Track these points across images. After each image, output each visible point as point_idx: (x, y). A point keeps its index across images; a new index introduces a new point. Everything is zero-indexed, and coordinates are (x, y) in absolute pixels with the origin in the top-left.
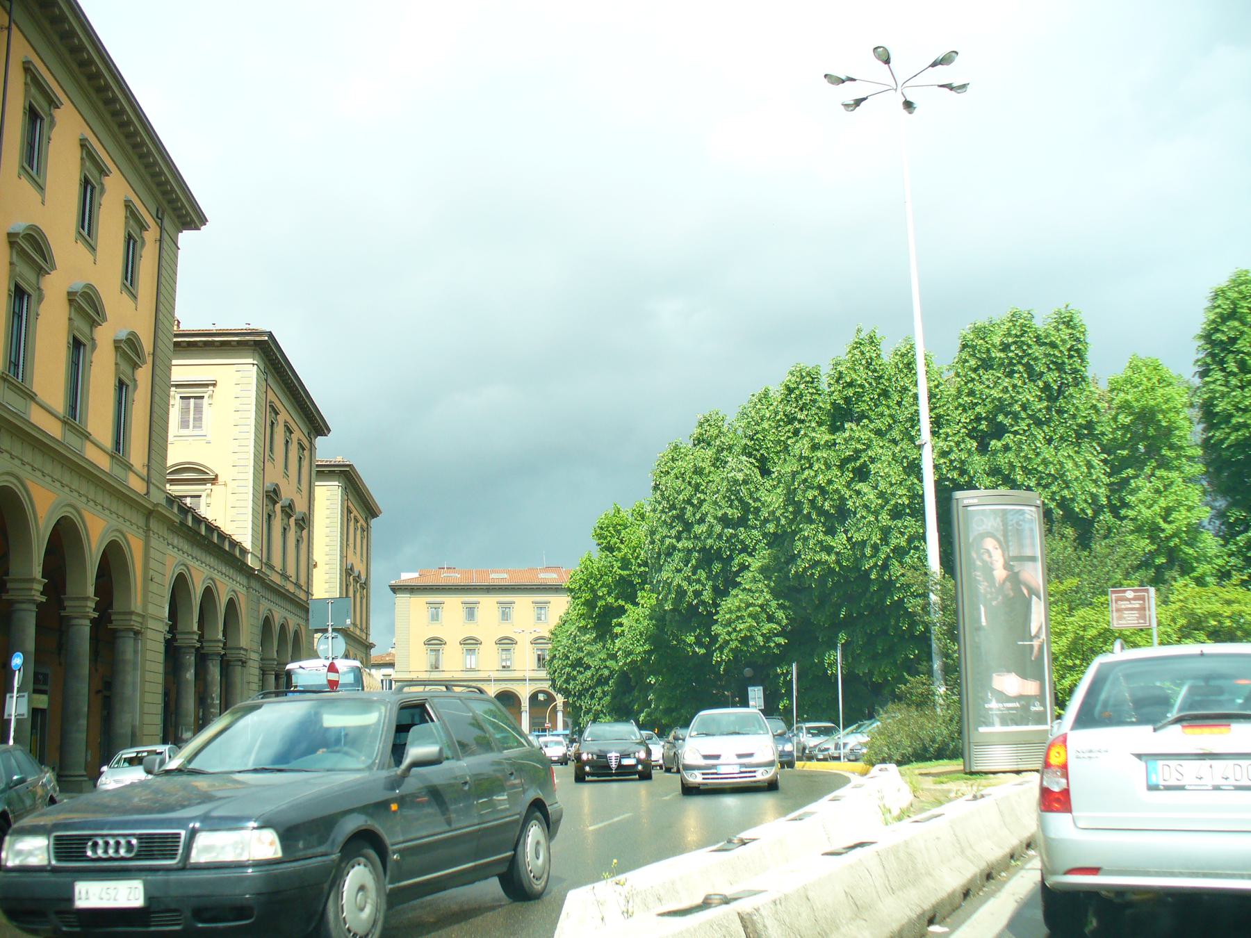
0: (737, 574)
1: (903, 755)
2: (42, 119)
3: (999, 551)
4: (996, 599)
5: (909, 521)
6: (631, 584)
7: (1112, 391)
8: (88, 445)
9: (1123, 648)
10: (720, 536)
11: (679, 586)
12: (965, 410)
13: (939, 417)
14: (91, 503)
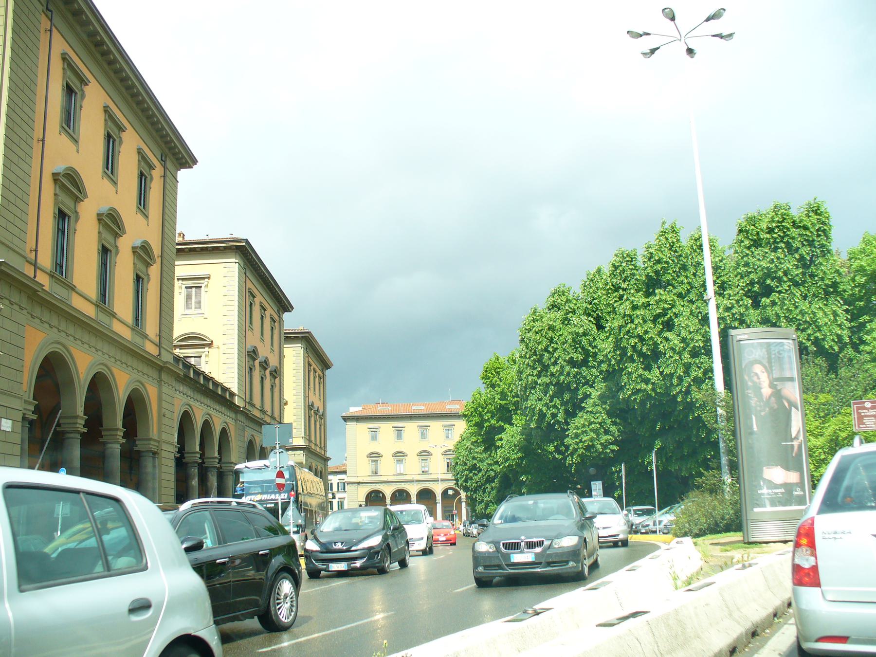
0: (582, 400)
1: (700, 530)
2: (76, 93)
3: (765, 374)
5: (704, 358)
7: (850, 259)
9: (861, 442)
10: (568, 373)
11: (540, 410)
12: (742, 277)
13: (723, 283)
14: (118, 363)
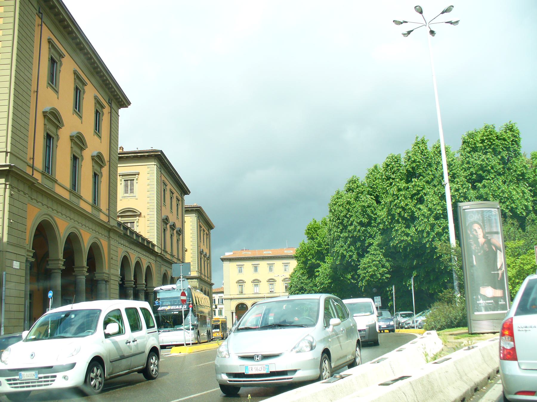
0: (368, 247)
1: (441, 326)
2: (57, 63)
3: (481, 230)
4: (480, 252)
5: (442, 220)
6: (322, 253)
7: (532, 159)
10: (359, 231)
11: (342, 253)
12: (465, 171)
13: (454, 174)
14: (84, 226)
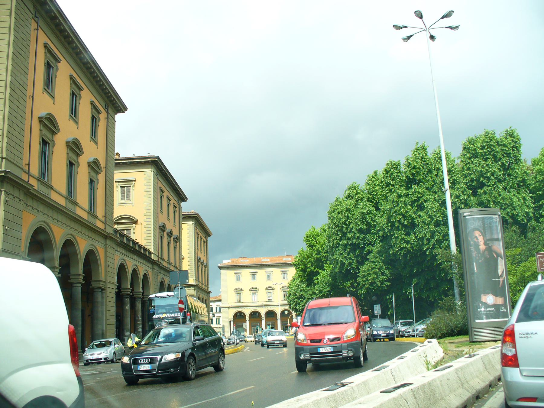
1: (442, 334)
2: (53, 68)
3: (482, 237)
7: (533, 165)
8: (78, 208)
10: (358, 238)
12: (466, 177)
14: (80, 233)
